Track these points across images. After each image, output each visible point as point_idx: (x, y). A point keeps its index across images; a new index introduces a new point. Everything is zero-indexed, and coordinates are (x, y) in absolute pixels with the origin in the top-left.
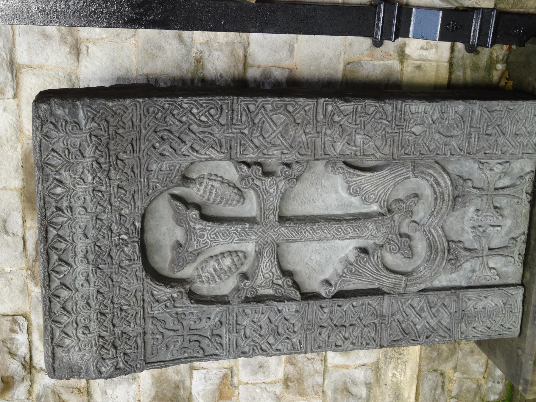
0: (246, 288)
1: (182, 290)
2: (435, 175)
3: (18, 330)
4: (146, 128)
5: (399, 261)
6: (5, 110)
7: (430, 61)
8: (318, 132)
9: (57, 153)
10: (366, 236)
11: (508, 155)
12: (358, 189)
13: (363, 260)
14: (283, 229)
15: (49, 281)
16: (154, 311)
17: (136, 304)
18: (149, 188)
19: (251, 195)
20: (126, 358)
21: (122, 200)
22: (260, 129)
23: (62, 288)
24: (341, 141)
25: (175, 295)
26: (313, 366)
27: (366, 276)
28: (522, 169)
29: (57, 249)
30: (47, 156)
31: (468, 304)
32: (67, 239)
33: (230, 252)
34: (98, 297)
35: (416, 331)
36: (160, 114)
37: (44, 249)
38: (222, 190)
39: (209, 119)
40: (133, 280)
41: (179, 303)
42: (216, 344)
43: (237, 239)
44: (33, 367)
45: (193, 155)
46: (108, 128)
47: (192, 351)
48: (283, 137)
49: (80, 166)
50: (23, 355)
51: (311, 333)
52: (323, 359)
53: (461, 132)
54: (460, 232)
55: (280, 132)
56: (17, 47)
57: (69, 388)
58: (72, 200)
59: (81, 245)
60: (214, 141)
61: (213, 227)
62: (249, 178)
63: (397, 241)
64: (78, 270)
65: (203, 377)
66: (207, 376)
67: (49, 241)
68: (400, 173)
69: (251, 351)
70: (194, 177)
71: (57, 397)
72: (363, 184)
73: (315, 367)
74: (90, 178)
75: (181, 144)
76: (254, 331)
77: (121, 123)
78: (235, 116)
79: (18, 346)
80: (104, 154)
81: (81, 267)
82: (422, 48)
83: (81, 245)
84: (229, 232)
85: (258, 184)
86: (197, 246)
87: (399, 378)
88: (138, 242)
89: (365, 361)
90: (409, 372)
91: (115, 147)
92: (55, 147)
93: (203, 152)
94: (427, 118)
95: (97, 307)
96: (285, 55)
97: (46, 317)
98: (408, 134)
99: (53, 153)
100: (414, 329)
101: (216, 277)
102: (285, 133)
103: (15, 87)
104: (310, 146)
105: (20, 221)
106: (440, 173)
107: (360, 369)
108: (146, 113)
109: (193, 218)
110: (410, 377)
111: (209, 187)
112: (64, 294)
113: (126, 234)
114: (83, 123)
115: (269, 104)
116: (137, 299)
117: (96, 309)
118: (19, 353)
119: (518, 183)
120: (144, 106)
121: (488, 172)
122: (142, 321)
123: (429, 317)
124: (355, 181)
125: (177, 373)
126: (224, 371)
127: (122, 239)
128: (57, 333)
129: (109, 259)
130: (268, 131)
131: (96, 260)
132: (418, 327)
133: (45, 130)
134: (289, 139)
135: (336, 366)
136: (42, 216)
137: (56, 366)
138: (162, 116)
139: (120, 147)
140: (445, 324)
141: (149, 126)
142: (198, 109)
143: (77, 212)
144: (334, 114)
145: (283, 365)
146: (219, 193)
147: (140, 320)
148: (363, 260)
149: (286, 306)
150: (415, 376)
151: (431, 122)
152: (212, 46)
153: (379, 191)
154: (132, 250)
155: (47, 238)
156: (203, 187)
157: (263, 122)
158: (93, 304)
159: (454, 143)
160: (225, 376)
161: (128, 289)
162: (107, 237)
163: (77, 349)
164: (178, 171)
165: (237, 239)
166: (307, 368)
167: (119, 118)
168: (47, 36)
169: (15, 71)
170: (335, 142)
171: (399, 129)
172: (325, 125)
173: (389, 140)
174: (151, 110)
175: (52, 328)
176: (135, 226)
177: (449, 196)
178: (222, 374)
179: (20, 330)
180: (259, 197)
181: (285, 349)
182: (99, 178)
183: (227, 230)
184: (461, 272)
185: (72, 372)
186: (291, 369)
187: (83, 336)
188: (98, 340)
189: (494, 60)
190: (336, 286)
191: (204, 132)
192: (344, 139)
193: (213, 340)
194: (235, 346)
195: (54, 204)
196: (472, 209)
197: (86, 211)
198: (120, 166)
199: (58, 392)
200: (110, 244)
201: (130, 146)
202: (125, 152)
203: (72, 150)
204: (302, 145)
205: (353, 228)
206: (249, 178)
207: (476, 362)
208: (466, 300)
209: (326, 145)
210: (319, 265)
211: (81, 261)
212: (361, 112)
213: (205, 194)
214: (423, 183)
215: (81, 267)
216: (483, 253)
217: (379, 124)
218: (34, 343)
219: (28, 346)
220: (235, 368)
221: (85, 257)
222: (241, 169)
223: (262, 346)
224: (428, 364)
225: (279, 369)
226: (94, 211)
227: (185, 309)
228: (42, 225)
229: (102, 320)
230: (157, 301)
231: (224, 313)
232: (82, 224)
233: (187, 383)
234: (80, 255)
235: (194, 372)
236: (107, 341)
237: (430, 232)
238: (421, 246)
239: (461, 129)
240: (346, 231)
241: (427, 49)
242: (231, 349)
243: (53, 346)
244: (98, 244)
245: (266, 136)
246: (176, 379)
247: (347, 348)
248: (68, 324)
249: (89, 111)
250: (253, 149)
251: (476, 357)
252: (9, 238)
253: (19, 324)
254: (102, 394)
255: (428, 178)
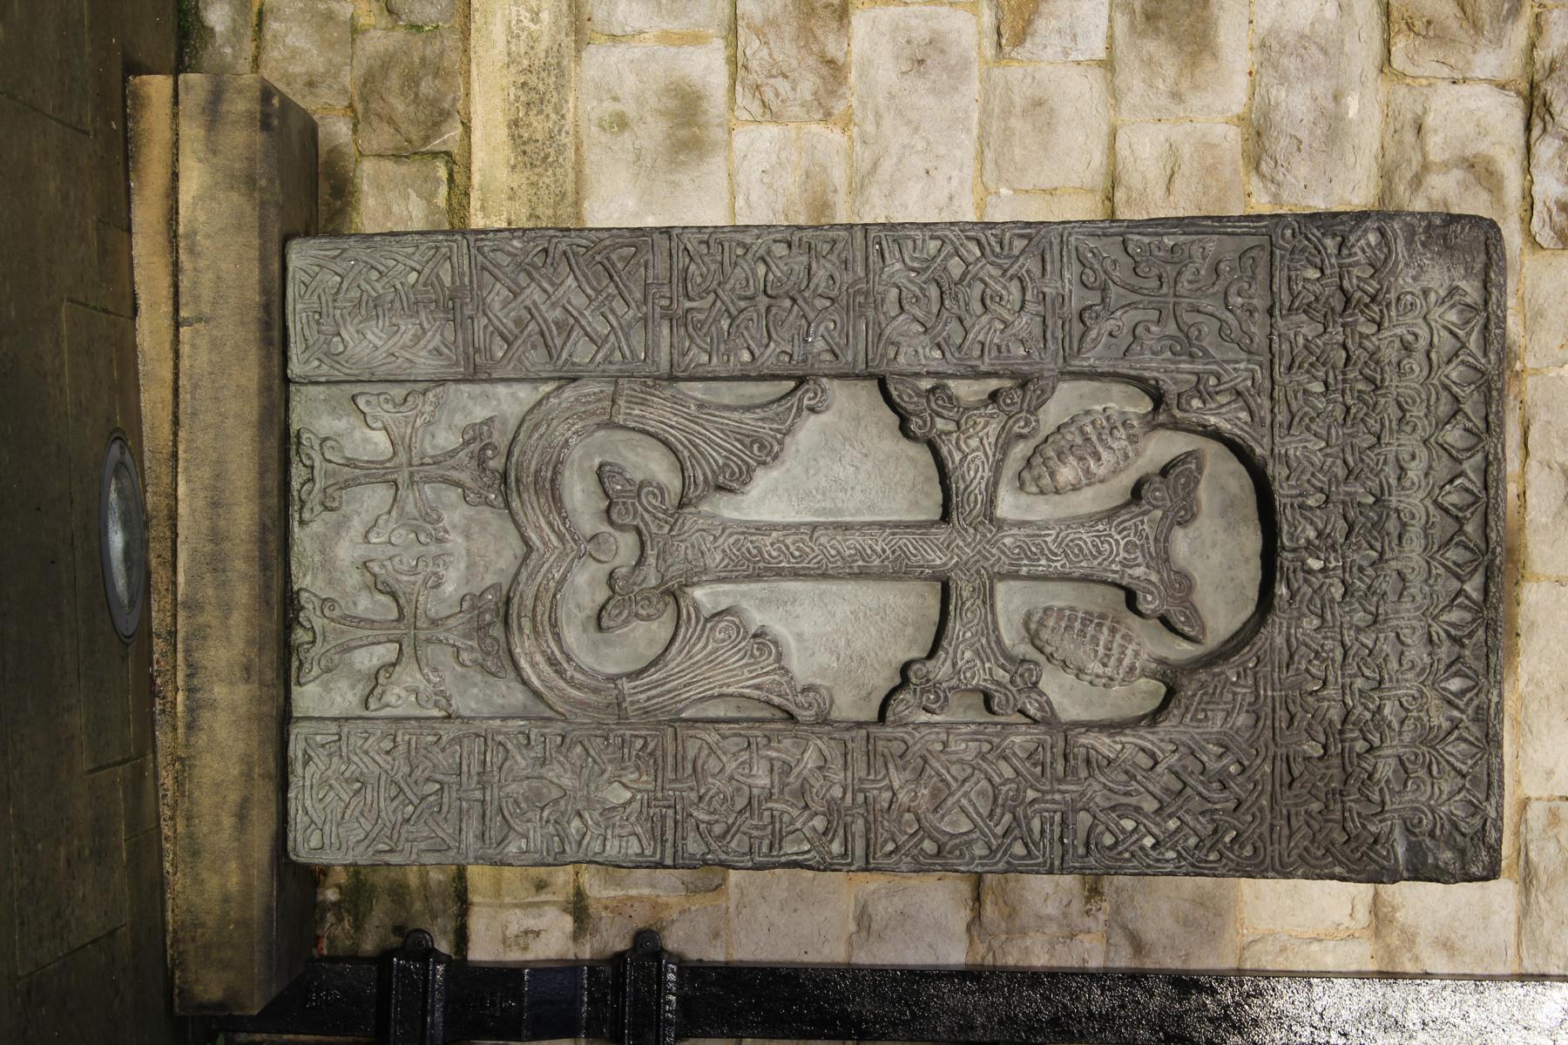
0: (1023, 414)
1: (1178, 414)
2: (562, 684)
3: (1554, 210)
4: (1261, 810)
5: (632, 457)
6: (1550, 773)
7: (517, 906)
8: (861, 790)
9: (1454, 768)
10: (731, 535)
11: (379, 733)
12: (757, 653)
13: (733, 473)
14: (938, 562)
15: (1486, 471)
16: (1246, 370)
17: (1290, 393)
18: (1255, 674)
19: (1010, 635)
20: (1318, 260)
21: (1317, 653)
22: (1000, 801)
23: (1458, 450)
24: (805, 772)
25: (1196, 403)
26: (771, 55)
27: (722, 431)
28: (326, 688)
29: (1466, 548)
30: (1475, 764)
31: (438, 337)
32: (1441, 571)
33: (1057, 492)
34: (1378, 426)
35: (578, 273)
36: (1227, 839)
37: (1494, 553)
38: (1081, 653)
39: (1117, 824)
40: (1301, 454)
41: (1187, 382)
42: (1096, 266)
43: (1048, 539)
44: (1525, 99)
45: (1153, 743)
46: (1344, 818)
47: (1156, 252)
48: (943, 780)
49: (1407, 738)
50: (1548, 139)
51: (855, 283)
52: (741, 72)
53: (508, 789)
54: (475, 529)
55: (951, 794)
56: (1513, 917)
57: (1436, 36)
58: (1427, 660)
59: (1413, 553)
60: (1103, 773)
61: (1105, 570)
62: (1021, 686)
63: (646, 516)
64: (1421, 494)
65: (1080, 39)
66: (1067, 43)
67: (1481, 570)
68: (653, 692)
69: (1006, 241)
70: (1143, 680)
71: (1469, 11)
72: (746, 665)
73: (765, 52)
74: (1387, 711)
75: (1180, 770)
76: (1001, 298)
77: (1316, 826)
78: (1057, 830)
79: (1557, 162)
80: (1355, 761)
81: (1414, 502)
82: (538, 934)
83: (1413, 553)
84: (1067, 556)
85: (1001, 672)
86: (1142, 522)
87: (523, 12)
88: (1283, 548)
89: (618, 54)
90: (498, 31)
91: (1330, 772)
92: (1459, 780)
93: (1129, 750)
94: (598, 824)
95: (1382, 401)
96: (880, 907)
97: (1499, 385)
98: (641, 786)
99: (1464, 768)
100: (581, 278)
101: (1094, 438)
102: (939, 790)
103: (1522, 828)
104: (880, 760)
105: (1532, 500)
106: (551, 689)
107: (628, 29)
108: (1259, 844)
109: (1151, 593)
110: (494, 15)
111: (1113, 662)
112: (1454, 436)
113: (1310, 571)
114: (1397, 833)
115: (981, 858)
116: (1289, 405)
117: (1384, 396)
118: (1557, 143)
119: (336, 657)
120: (1263, 862)
121: (422, 684)
122: (1275, 346)
123: (543, 308)
124: (767, 673)
125: (1150, 60)
126: (1022, 53)
127: (1318, 558)
128: (1473, 342)
129: (1351, 514)
130: (979, 794)
131: (1380, 517)
132: (570, 281)
133: (1477, 821)
134: (930, 777)
135: (697, 39)
136: (1495, 631)
137: (1483, 257)
138: (1223, 836)
139: (1319, 773)
140: (498, 285)
141: (1254, 816)
142: (1142, 848)
143: (1418, 633)
144: (825, 834)
145: (854, 57)
146: (1088, 647)
147: (1281, 352)
148: (733, 473)
149: (923, 361)
150: (477, 16)
151: (586, 815)
152: (1060, 926)
153: (704, 647)
154: (1298, 531)
155: (1487, 579)
156: (1126, 662)
157: (991, 815)
158: (1394, 412)
159: (523, 763)
160: (1020, 38)
161: (1306, 435)
162: (1355, 570)
163: (1432, 297)
164: (1187, 708)
165: (1048, 539)
166: (790, 49)
167: (1320, 837)
168: (1444, 945)
169: (1522, 862)
170: (820, 768)
171: (664, 798)
172: (847, 809)
173: (689, 770)
174: (1248, 851)
175: (1485, 355)
176: (1288, 586)
177: (520, 628)
178: (1028, 44)
179: (1549, 210)
180: (999, 641)
181: (919, 243)
182: (1367, 709)
183: (1070, 561)
184: (460, 420)
185: (1445, 239)
186: (833, 49)
187: (1417, 330)
188: (1382, 317)
189: (348, 911)
190: (800, 410)
191: (1127, 794)
192: (797, 776)
193: (1103, 277)
194: (1048, 257)
195: (1467, 653)
196: (450, 588)
197: (1398, 635)
198: (1320, 729)
199: (1465, 24)
200: (1349, 553)
201: (1296, 773)
202: (1308, 759)
203: (1422, 773)
204: (899, 761)
205: (763, 558)
206: (1021, 686)
207: (295, 54)
208: (446, 351)
209: (841, 762)
210: (833, 450)
211: (1413, 517)
212: (762, 838)
213: (1122, 646)
214: (586, 659)
215: (1414, 502)
216: (411, 475)
217: (714, 812)
218: (1518, 167)
219: (1533, 162)
220: (990, 52)
221: (1404, 525)
222: (1041, 709)
223: (979, 254)
224: (442, 53)
225: (867, 45)
226: (1382, 636)
227: (1173, 367)
228: (1496, 609)
229: (1373, 366)
230: (1239, 394)
231: (1075, 347)
232: (1408, 606)
233: (1121, 22)
234: (1415, 531)
235: (1102, 55)
236: (1362, 312)
237: (561, 538)
238: (579, 493)
239: (507, 796)
240: (779, 549)
241: (526, 932)
242: (1056, 248)
243: (1486, 310)
244: (1374, 554)
245: (984, 783)
246: (1155, 43)
247: (758, 237)
248: (1449, 361)
249: (1384, 858)
250: (1015, 754)
251: (297, 68)
252: (1561, 459)
253: (1552, 228)
254: (1350, 6)
255: (578, 676)
